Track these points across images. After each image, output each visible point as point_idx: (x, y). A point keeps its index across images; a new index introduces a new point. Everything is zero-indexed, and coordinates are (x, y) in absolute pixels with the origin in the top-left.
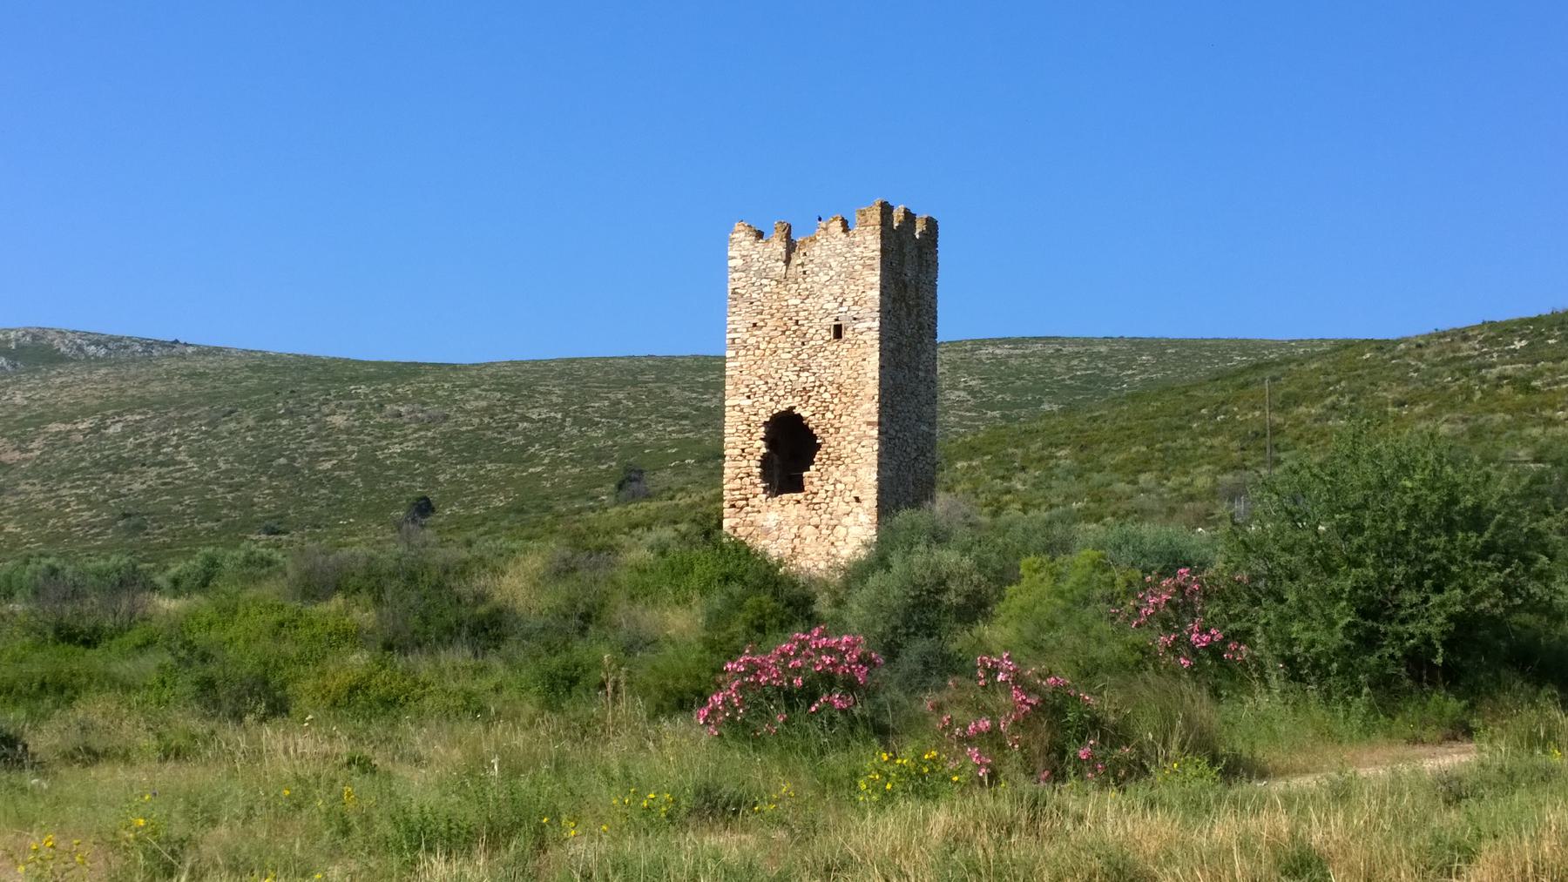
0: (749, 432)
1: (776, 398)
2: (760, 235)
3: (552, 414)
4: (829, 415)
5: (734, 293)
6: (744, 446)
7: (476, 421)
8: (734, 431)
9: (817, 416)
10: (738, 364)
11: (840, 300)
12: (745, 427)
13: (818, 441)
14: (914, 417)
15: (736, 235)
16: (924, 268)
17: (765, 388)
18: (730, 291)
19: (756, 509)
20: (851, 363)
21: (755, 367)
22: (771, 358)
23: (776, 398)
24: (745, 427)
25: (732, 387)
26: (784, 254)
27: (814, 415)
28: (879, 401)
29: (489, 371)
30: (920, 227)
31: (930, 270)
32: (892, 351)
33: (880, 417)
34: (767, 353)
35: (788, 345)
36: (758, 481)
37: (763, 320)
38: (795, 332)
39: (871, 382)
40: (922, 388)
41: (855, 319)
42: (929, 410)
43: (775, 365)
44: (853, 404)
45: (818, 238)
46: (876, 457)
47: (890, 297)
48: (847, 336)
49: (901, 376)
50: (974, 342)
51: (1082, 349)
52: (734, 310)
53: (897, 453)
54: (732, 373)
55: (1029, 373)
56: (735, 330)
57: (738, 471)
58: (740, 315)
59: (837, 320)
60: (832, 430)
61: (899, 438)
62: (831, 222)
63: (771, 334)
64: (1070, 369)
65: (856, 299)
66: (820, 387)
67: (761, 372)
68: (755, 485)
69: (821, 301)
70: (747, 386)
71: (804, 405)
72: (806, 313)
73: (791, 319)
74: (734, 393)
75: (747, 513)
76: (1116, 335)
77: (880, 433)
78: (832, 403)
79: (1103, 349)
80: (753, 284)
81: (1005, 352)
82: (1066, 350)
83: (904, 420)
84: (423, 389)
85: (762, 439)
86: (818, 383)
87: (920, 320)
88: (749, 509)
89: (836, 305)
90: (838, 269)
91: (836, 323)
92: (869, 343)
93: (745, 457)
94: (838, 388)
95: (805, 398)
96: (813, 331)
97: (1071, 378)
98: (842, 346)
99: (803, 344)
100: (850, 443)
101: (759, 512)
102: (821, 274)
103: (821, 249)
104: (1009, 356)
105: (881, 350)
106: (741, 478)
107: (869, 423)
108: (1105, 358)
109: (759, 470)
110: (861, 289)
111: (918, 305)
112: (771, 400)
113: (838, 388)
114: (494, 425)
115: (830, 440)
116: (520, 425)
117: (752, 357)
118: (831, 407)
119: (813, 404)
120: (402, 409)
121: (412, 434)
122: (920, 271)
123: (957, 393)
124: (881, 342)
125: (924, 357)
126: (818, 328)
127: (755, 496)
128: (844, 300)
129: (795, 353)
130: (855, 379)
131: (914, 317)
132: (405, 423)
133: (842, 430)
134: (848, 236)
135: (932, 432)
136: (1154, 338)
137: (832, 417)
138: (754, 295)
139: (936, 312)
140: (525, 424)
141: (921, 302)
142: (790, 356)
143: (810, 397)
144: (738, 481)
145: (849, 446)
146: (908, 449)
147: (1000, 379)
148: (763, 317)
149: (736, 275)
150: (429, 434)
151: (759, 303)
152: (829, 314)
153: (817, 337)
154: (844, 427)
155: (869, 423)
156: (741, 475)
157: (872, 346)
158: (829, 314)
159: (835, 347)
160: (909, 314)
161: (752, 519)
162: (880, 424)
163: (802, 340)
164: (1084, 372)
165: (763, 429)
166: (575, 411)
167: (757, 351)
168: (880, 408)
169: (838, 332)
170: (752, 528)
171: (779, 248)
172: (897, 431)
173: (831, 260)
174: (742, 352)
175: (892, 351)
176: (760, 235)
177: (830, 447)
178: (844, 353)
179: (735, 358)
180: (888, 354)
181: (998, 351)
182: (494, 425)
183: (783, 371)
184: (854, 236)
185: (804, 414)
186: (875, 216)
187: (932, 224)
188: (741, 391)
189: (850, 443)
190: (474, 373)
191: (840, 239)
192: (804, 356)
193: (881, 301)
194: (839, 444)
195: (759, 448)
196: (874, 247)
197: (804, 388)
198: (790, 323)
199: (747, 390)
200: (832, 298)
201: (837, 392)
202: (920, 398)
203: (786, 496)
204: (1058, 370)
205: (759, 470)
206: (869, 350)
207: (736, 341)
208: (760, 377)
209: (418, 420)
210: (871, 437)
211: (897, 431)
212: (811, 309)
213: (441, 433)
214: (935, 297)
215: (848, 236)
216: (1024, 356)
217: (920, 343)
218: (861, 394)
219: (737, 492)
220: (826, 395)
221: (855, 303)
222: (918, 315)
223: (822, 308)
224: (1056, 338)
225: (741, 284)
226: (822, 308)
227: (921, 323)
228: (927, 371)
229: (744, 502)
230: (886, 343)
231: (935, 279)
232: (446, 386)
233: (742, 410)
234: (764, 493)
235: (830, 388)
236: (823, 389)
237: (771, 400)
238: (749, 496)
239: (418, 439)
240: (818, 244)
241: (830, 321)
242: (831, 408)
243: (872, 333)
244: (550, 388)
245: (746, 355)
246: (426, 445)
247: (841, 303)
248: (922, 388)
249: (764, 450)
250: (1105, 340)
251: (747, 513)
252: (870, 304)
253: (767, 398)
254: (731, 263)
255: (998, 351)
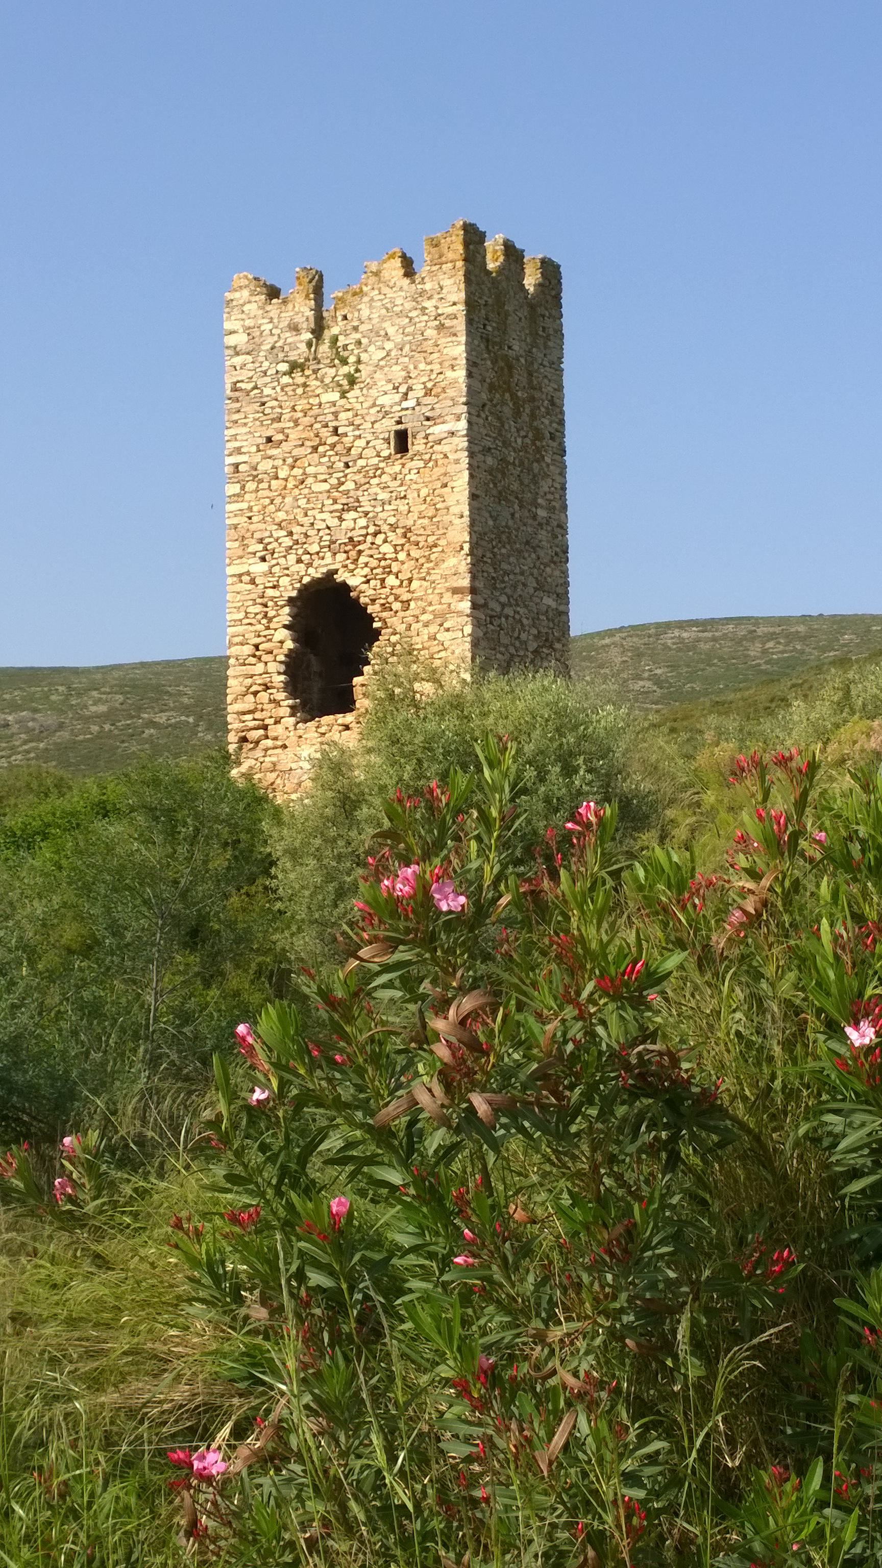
0: (265, 616)
1: (306, 558)
2: (273, 293)
3: (183, 718)
4: (391, 581)
5: (235, 389)
6: (257, 640)
7: (95, 729)
8: (241, 615)
9: (372, 583)
10: (244, 505)
11: (403, 389)
12: (258, 608)
13: (376, 625)
14: (532, 583)
15: (237, 295)
16: (540, 341)
17: (288, 542)
18: (228, 387)
19: (279, 743)
20: (424, 492)
21: (272, 508)
22: (297, 491)
23: (306, 558)
24: (258, 608)
25: (237, 544)
26: (312, 319)
27: (368, 582)
28: (471, 553)
29: (116, 674)
30: (531, 280)
31: (550, 344)
32: (490, 471)
33: (474, 578)
34: (290, 485)
35: (322, 469)
36: (281, 696)
37: (282, 431)
38: (333, 446)
39: (457, 521)
40: (543, 535)
41: (428, 419)
42: (557, 573)
43: (302, 502)
44: (429, 560)
45: (365, 289)
46: (468, 646)
47: (483, 381)
48: (416, 448)
49: (506, 514)
50: (658, 625)
51: (778, 630)
52: (236, 417)
53: (505, 640)
54: (235, 521)
55: (721, 659)
56: (238, 451)
57: (250, 680)
58: (245, 424)
59: (399, 422)
60: (396, 606)
61: (507, 617)
62: (385, 262)
63: (296, 452)
64: (765, 652)
65: (429, 385)
66: (375, 534)
67: (281, 515)
68: (277, 703)
69: (374, 392)
70: (261, 541)
71: (351, 567)
72: (350, 414)
73: (326, 426)
74: (240, 553)
75: (266, 750)
76: (815, 614)
77: (474, 606)
78: (396, 560)
79: (801, 629)
80: (265, 373)
81: (693, 635)
82: (760, 631)
83: (515, 587)
84: (34, 693)
85: (285, 627)
86: (372, 529)
87: (535, 424)
88: (269, 743)
89: (397, 397)
90: (399, 339)
91: (399, 427)
92: (452, 457)
93: (259, 658)
94: (405, 535)
95: (353, 554)
96: (361, 443)
97: (767, 663)
98: (410, 465)
99: (347, 466)
100: (426, 625)
101: (284, 747)
102: (372, 349)
103: (371, 307)
104: (698, 640)
105: (471, 467)
106: (255, 694)
107: (455, 591)
108: (804, 639)
109: (282, 678)
110: (436, 367)
111: (532, 399)
112: (299, 561)
113: (405, 535)
114: (116, 732)
115: (393, 621)
116: (147, 731)
117: (267, 493)
118: (395, 567)
119: (366, 565)
120: (10, 718)
121: (21, 745)
122: (534, 344)
123: (641, 683)
124: (471, 455)
125: (545, 485)
126: (370, 437)
127: (277, 722)
128: (410, 389)
129: (334, 481)
130: (431, 518)
131: (525, 417)
132: (13, 735)
133: (412, 604)
134: (413, 282)
135: (562, 608)
136: (856, 615)
137: (397, 583)
138: (267, 391)
139: (562, 413)
140: (152, 731)
141: (537, 395)
142: (326, 486)
143: (360, 552)
144: (250, 698)
145: (426, 631)
146: (524, 636)
147: (688, 666)
148: (281, 425)
149: (238, 360)
150: (42, 745)
151: (275, 403)
152: (387, 413)
153: (369, 452)
154: (416, 599)
155: (455, 591)
156: (254, 688)
157: (457, 462)
158: (387, 413)
159: (397, 468)
160: (517, 414)
161: (274, 759)
162: (473, 591)
163: (345, 459)
164: (780, 655)
165: (287, 610)
166: (209, 714)
167: (273, 482)
168: (473, 564)
169: (402, 441)
170: (274, 775)
171: (303, 309)
172: (503, 606)
173: (387, 325)
174: (251, 486)
175: (490, 471)
176: (273, 293)
177: (395, 634)
178: (413, 476)
179: (238, 497)
180: (483, 475)
181: (685, 635)
182: (116, 732)
183: (315, 512)
184: (423, 282)
185: (352, 582)
186: (456, 248)
187: (551, 271)
188: (250, 549)
189: (426, 625)
190: (99, 676)
191: (401, 289)
192: (350, 485)
193: (469, 387)
194: (409, 628)
195: (282, 642)
196: (454, 297)
197: (351, 539)
198: (324, 433)
199: (261, 547)
200: (391, 386)
201: (403, 541)
202: (542, 553)
203: (327, 719)
204: (752, 653)
205: (282, 678)
206: (451, 468)
207: (241, 468)
208: (279, 525)
209: (29, 731)
210: (459, 613)
211: (503, 606)
212: (358, 406)
213: (55, 744)
214: (560, 388)
215: (413, 282)
216: (714, 639)
217: (538, 461)
218: (442, 542)
219: (249, 717)
220: (387, 549)
221: (428, 392)
222: (533, 416)
223: (374, 405)
224: (748, 618)
225: (244, 375)
226: (374, 405)
227: (537, 429)
228: (552, 509)
229: (261, 732)
230: (480, 457)
231: (560, 358)
232: (61, 688)
233: (253, 582)
234: (292, 715)
235: (391, 536)
236: (380, 537)
237: (299, 561)
238: (267, 721)
239: (28, 752)
240: (366, 299)
241: (388, 426)
242: (395, 570)
243: (455, 440)
244: (181, 688)
245: (257, 491)
246: (37, 758)
247: (406, 394)
248: (543, 535)
249: (290, 645)
250: (805, 619)
251: (266, 750)
252: (451, 393)
253: (292, 558)
254: (230, 340)
255: (685, 635)
